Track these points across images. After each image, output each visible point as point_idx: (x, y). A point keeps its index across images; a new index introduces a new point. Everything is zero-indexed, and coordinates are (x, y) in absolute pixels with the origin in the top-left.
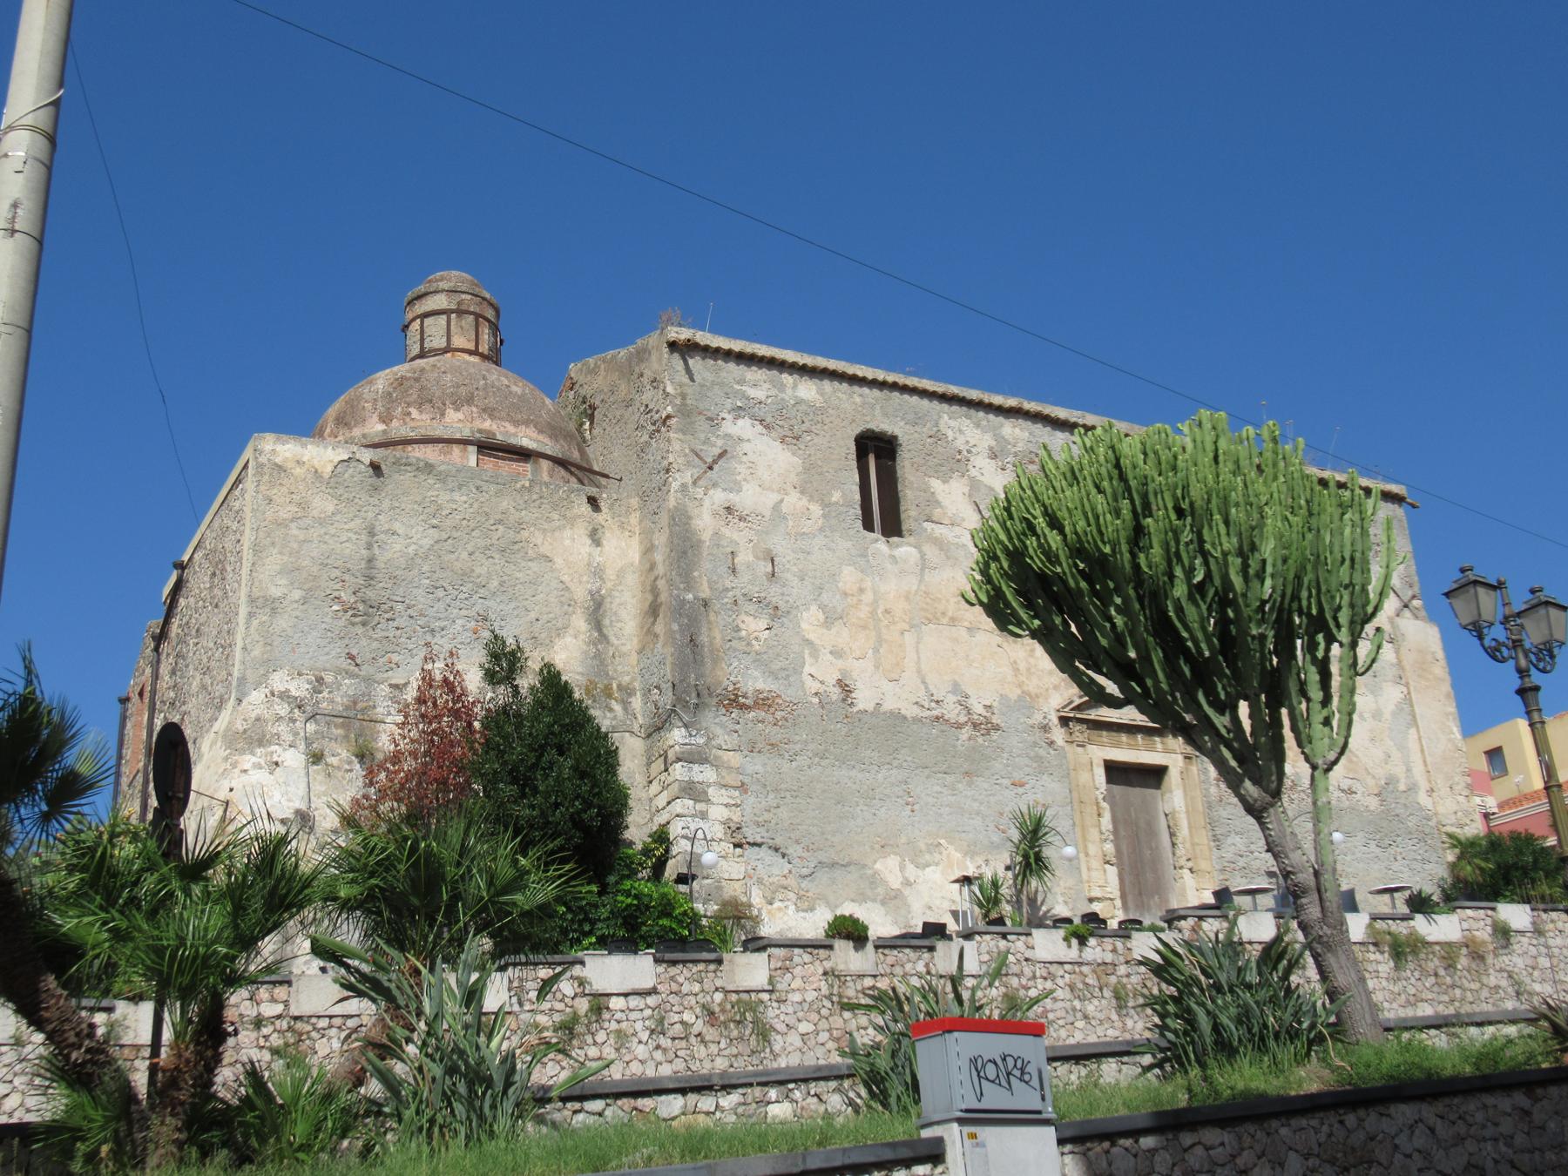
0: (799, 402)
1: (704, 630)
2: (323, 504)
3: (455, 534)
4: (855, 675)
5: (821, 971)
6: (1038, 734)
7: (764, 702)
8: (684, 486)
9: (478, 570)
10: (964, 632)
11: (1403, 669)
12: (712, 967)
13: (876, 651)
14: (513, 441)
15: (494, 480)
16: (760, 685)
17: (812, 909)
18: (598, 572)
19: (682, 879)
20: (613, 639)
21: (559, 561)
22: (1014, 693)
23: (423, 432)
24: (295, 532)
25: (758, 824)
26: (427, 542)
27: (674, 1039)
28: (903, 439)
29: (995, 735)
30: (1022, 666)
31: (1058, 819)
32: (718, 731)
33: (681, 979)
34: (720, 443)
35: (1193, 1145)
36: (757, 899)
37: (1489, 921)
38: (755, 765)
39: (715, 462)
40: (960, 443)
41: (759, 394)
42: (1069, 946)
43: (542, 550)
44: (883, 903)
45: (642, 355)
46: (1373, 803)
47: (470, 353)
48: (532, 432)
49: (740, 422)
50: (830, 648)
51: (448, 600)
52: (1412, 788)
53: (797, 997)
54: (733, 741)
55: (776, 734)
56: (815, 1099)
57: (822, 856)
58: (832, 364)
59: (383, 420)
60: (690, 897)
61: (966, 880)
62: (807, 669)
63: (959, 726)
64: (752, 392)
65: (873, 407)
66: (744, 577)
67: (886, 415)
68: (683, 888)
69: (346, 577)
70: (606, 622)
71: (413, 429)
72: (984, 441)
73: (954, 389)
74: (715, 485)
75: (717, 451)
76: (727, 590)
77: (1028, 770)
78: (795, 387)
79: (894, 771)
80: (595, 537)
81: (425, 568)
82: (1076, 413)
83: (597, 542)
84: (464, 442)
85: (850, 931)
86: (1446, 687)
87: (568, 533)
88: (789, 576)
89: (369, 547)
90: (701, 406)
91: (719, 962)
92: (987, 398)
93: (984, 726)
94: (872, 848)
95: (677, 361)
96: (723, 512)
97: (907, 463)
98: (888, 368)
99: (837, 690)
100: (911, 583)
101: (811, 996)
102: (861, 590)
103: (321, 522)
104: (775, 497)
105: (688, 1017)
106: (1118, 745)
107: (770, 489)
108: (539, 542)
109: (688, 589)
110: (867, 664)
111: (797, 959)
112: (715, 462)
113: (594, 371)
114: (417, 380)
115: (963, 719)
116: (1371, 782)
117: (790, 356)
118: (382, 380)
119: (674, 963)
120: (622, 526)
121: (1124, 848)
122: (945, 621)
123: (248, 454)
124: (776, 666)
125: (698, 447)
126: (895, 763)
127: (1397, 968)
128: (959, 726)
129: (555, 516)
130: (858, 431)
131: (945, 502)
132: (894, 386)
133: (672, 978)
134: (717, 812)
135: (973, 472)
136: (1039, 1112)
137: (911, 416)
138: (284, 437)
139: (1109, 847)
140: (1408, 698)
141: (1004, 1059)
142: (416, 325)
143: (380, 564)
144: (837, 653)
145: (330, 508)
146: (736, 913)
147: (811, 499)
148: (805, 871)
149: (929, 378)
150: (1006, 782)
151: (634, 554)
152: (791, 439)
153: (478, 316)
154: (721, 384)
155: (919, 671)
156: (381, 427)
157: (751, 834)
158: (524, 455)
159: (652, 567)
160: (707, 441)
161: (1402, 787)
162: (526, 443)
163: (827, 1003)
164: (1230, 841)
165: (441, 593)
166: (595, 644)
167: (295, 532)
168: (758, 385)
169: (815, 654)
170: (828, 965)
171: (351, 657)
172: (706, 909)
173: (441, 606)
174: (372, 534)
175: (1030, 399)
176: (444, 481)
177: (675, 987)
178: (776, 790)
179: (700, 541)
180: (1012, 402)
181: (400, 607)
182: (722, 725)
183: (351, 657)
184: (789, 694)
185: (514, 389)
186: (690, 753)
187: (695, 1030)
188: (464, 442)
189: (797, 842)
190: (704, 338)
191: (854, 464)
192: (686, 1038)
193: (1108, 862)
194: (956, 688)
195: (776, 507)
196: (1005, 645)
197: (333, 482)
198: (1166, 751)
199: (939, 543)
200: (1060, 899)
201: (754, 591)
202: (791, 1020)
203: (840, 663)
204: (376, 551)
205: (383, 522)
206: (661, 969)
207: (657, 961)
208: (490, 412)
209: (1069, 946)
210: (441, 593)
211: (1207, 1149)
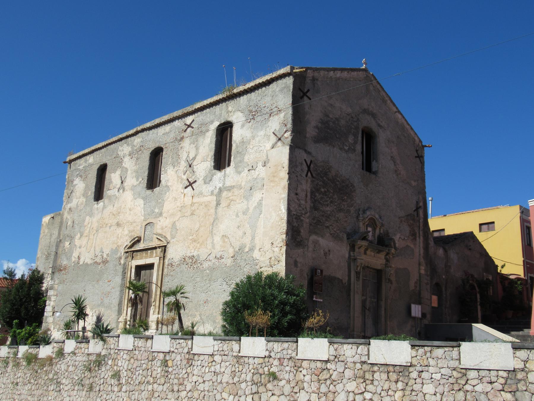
93: (105, 262)
150: (106, 281)
161: (247, 250)
180: (135, 130)
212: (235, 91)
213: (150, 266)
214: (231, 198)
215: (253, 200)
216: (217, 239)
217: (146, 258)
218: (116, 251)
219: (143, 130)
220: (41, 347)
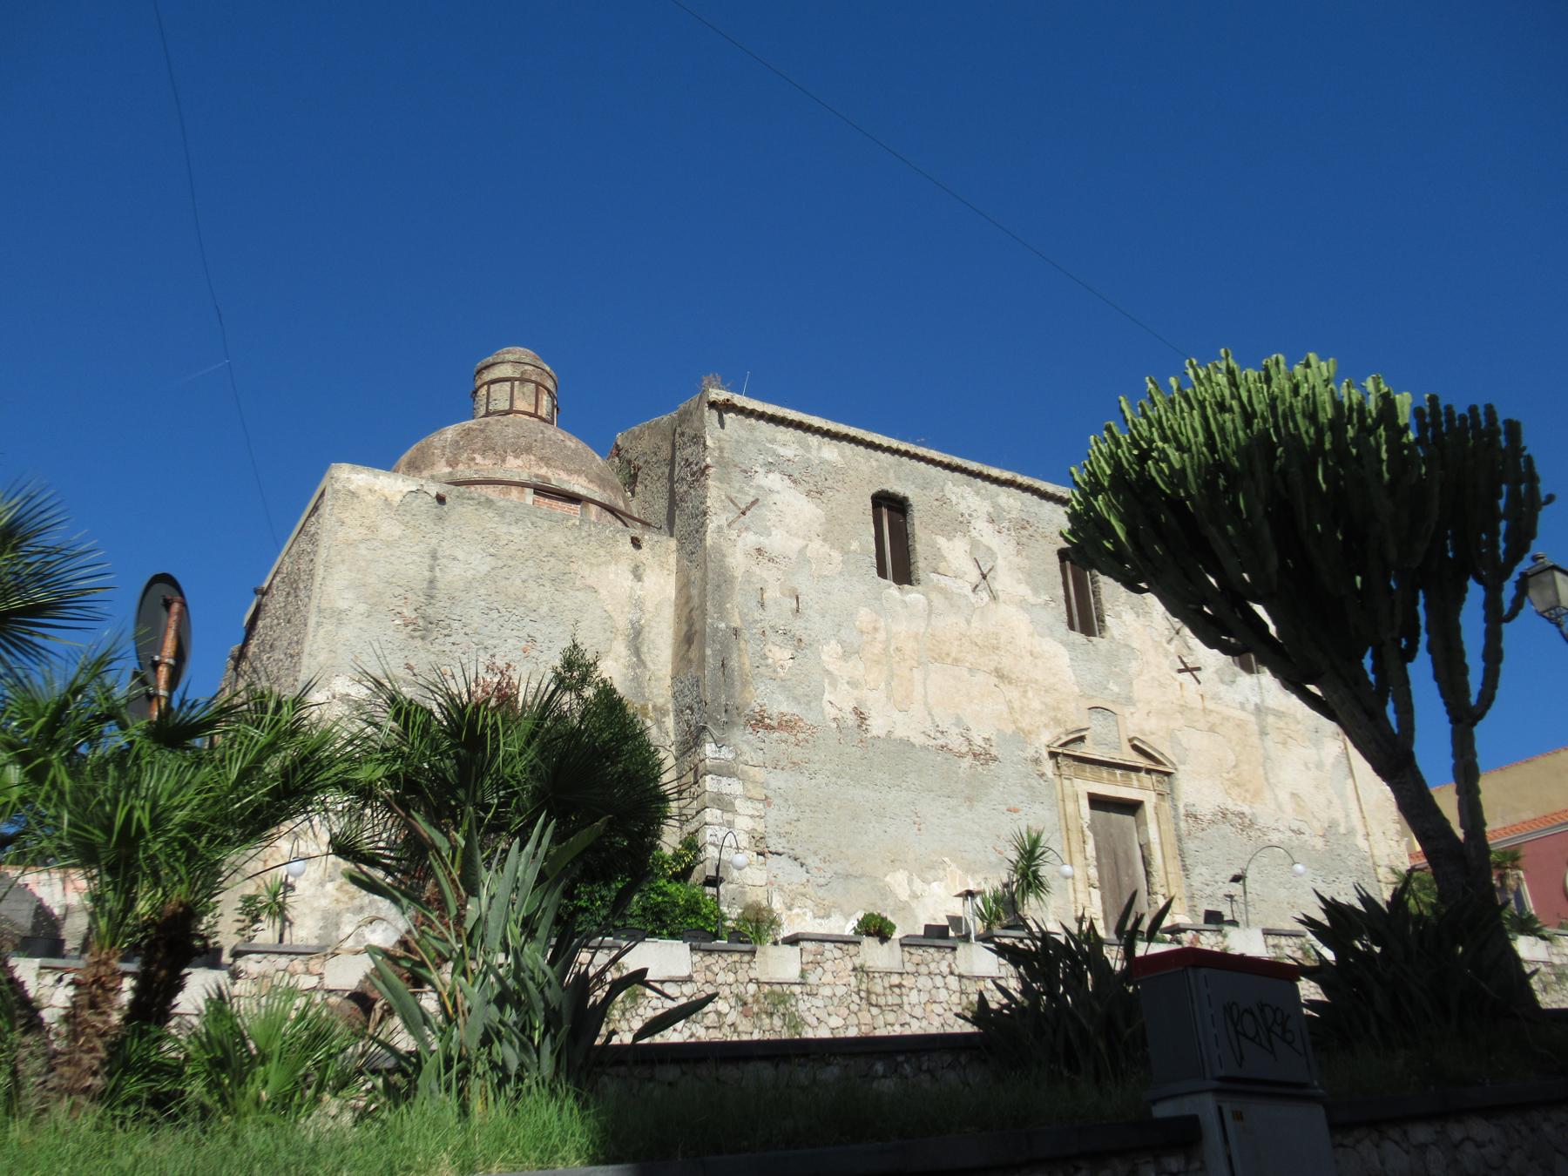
0: (823, 462)
1: (735, 656)
2: (390, 528)
3: (511, 563)
6: (1031, 767)
7: (787, 725)
8: (720, 528)
9: (530, 596)
10: (965, 672)
12: (747, 958)
13: (888, 684)
14: (566, 487)
15: (548, 517)
16: (784, 708)
18: (638, 605)
19: (714, 882)
20: (649, 664)
21: (603, 592)
22: (1009, 729)
23: (486, 474)
24: (364, 552)
25: (779, 835)
26: (484, 568)
27: (708, 1028)
28: (913, 499)
29: (993, 765)
30: (1016, 705)
31: (1052, 841)
32: (745, 748)
33: (716, 969)
34: (753, 492)
35: (1463, 1141)
36: (777, 905)
38: (778, 780)
39: (748, 508)
40: (962, 508)
41: (788, 452)
43: (589, 582)
45: (685, 417)
46: (1319, 843)
47: (530, 415)
48: (583, 480)
49: (771, 476)
51: (501, 621)
52: (1351, 832)
53: (827, 991)
54: (758, 758)
55: (798, 754)
56: (927, 1077)
57: (836, 867)
59: (449, 464)
60: (717, 899)
61: (969, 894)
62: (827, 697)
63: (962, 756)
64: (781, 451)
65: (887, 471)
66: (772, 610)
67: (898, 478)
68: (710, 890)
69: (409, 595)
70: (644, 649)
71: (476, 472)
72: (985, 507)
73: (957, 461)
74: (747, 529)
75: (751, 499)
76: (756, 621)
78: (819, 448)
79: (904, 793)
80: (637, 574)
81: (482, 591)
83: (638, 577)
84: (523, 485)
85: (876, 928)
87: (612, 568)
89: (432, 569)
90: (737, 460)
91: (753, 953)
92: (987, 470)
93: (983, 757)
95: (715, 413)
96: (754, 553)
97: (917, 522)
98: (903, 439)
99: (853, 717)
101: (841, 990)
102: (876, 629)
103: (388, 544)
104: (801, 542)
106: (1099, 780)
108: (586, 574)
109: (721, 619)
111: (828, 954)
112: (748, 508)
113: (638, 438)
114: (482, 431)
115: (964, 749)
117: (816, 421)
118: (450, 432)
119: (710, 952)
120: (661, 567)
121: (1105, 872)
122: (949, 661)
123: (325, 483)
124: (799, 691)
125: (733, 495)
126: (904, 785)
128: (962, 756)
129: (602, 552)
130: (874, 490)
131: (950, 557)
132: (906, 454)
133: (708, 968)
134: (743, 823)
135: (974, 533)
136: (1303, 1086)
137: (920, 481)
138: (359, 468)
139: (1093, 872)
141: (1262, 1011)
142: (484, 391)
143: (440, 585)
145: (398, 532)
147: (832, 546)
148: (822, 881)
149: (937, 449)
150: (1004, 808)
151: (671, 591)
152: (816, 493)
153: (538, 384)
154: (755, 442)
155: (926, 704)
156: (448, 470)
157: (774, 843)
158: (573, 498)
159: (689, 599)
160: (741, 490)
161: (1342, 830)
162: (583, 492)
163: (855, 998)
164: (1197, 871)
165: (495, 614)
166: (634, 669)
167: (364, 552)
168: (787, 443)
170: (858, 962)
171: (409, 667)
172: (732, 912)
173: (494, 626)
174: (434, 557)
175: (1023, 473)
176: (502, 516)
177: (710, 976)
178: (797, 805)
181: (456, 625)
182: (748, 742)
183: (409, 667)
184: (810, 718)
185: (568, 443)
186: (719, 767)
187: (729, 1020)
188: (523, 485)
189: (815, 853)
190: (740, 400)
191: (871, 519)
192: (720, 1028)
193: (1091, 885)
194: (958, 721)
195: (802, 551)
197: (400, 510)
198: (1142, 788)
199: (943, 591)
201: (780, 624)
202: (822, 1014)
204: (438, 573)
205: (445, 549)
206: (697, 958)
207: (692, 949)
208: (546, 460)
211: (1479, 1146)
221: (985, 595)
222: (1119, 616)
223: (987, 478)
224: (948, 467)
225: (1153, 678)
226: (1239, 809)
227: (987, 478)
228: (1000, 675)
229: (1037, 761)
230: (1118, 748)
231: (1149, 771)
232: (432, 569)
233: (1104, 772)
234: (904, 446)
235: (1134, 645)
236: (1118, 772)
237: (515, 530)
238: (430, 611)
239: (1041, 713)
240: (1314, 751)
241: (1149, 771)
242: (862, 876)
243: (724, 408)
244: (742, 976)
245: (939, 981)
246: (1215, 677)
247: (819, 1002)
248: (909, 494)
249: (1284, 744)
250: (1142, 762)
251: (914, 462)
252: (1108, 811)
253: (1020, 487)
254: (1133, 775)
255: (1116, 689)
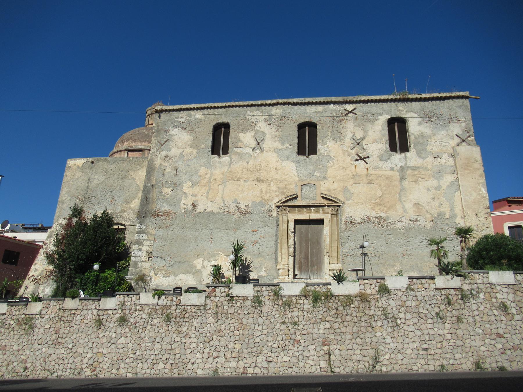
0: (196, 119)
1: (151, 194)
2: (79, 174)
4: (198, 201)
5: (58, 308)
9: (115, 185)
11: (456, 167)
13: (208, 193)
14: (138, 147)
16: (166, 208)
17: (169, 276)
21: (137, 179)
22: (258, 200)
25: (157, 251)
26: (103, 179)
30: (264, 190)
32: (150, 224)
34: (167, 137)
37: (378, 285)
38: (160, 233)
42: (154, 298)
44: (193, 274)
46: (428, 225)
50: (191, 194)
53: (47, 316)
55: (168, 223)
57: (176, 259)
58: (207, 105)
62: (183, 201)
64: (180, 120)
66: (167, 176)
74: (163, 151)
77: (259, 226)
82: (301, 99)
86: (481, 171)
87: (141, 170)
88: (182, 174)
89: (88, 183)
92: (264, 102)
93: (244, 213)
94: (194, 256)
100: (225, 169)
102: (206, 174)
103: (77, 179)
105: (12, 323)
106: (302, 213)
107: (181, 148)
110: (204, 198)
116: (428, 216)
127: (314, 307)
129: (138, 166)
132: (229, 106)
134: (145, 248)
140: (457, 179)
143: (90, 187)
144: (194, 195)
146: (142, 278)
148: (170, 265)
150: (250, 230)
155: (222, 197)
158: (140, 150)
161: (447, 216)
162: (142, 147)
163: (57, 318)
164: (347, 244)
168: (182, 117)
169: (186, 197)
174: (89, 180)
175: (282, 98)
176: (109, 163)
178: (165, 240)
179: (155, 168)
180: (275, 101)
181: (93, 198)
182: (151, 222)
186: (140, 231)
187: (12, 326)
189: (169, 256)
190: (165, 107)
194: (235, 201)
195: (181, 153)
196: (258, 184)
200: (263, 270)
203: (194, 198)
206: (9, 307)
209: (154, 298)
210: (104, 193)
212: (410, 96)
213: (321, 222)
214: (418, 176)
215: (445, 180)
216: (409, 206)
217: (311, 213)
218: (264, 202)
219: (289, 104)
220: (102, 299)
221: (258, 151)
222: (325, 144)
223: (266, 105)
224: (248, 106)
225: (340, 166)
226: (378, 215)
227: (266, 105)
228: (259, 180)
229: (270, 211)
230: (315, 199)
231: (328, 206)
232: (88, 183)
233: (305, 210)
234: (227, 104)
235: (332, 154)
236: (313, 209)
237: (112, 166)
238: (87, 196)
239: (276, 191)
240: (436, 181)
241: (328, 206)
242: (185, 262)
243: (159, 112)
244: (21, 313)
245: (90, 312)
246: (378, 159)
247: (43, 320)
248: (229, 121)
249: (416, 181)
250: (326, 202)
251: (234, 108)
252: (310, 224)
253: (281, 104)
254: (321, 209)
255: (318, 175)
